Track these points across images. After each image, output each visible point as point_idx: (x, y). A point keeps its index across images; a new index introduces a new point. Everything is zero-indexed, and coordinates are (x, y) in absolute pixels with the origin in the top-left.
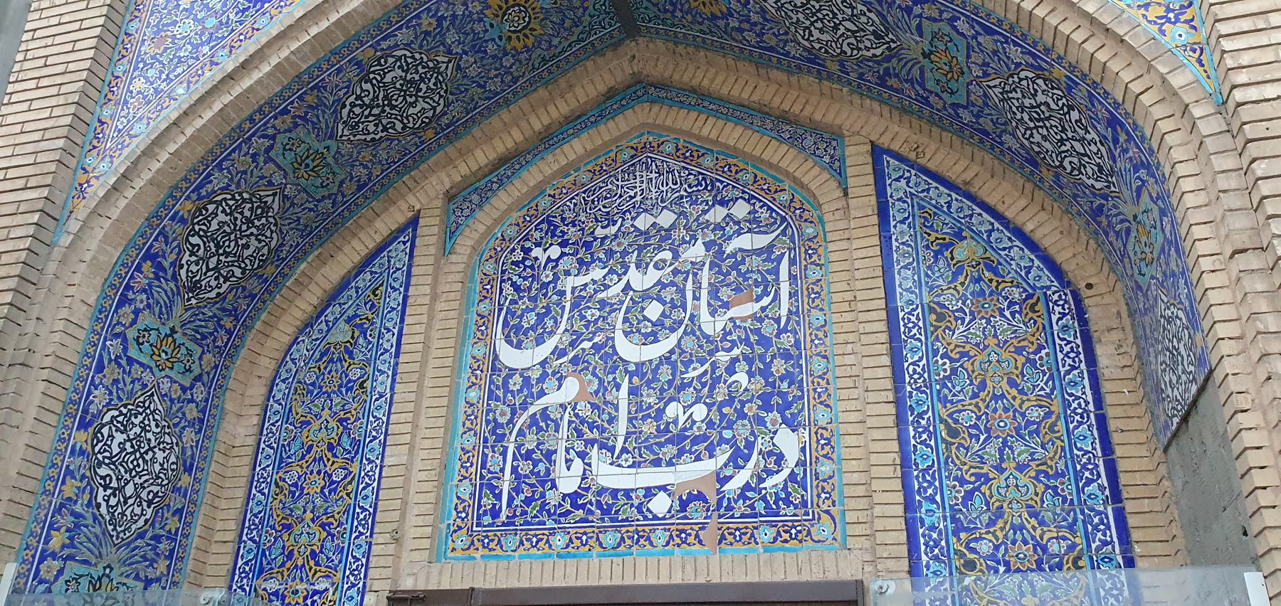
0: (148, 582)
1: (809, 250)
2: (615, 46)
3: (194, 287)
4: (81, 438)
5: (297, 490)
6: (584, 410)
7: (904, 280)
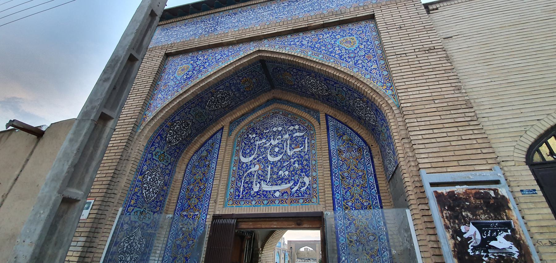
0: (154, 213)
1: (312, 137)
2: (270, 91)
3: (170, 142)
4: (140, 177)
6: (260, 172)
7: (332, 143)
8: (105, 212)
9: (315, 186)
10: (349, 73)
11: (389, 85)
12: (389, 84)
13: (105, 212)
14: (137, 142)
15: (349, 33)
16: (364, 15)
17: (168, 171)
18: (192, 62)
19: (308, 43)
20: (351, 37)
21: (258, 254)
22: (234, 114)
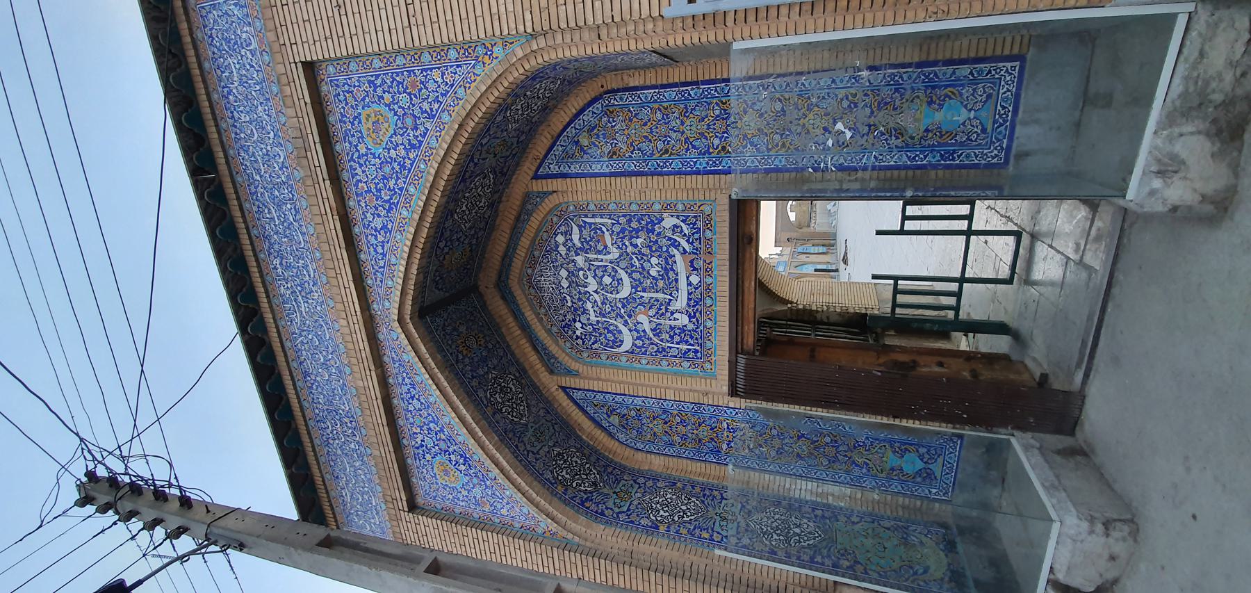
0: (723, 498)
1: (582, 210)
2: (481, 295)
3: (595, 484)
4: (662, 528)
5: (684, 437)
6: (652, 312)
7: (597, 168)
8: (723, 576)
9: (680, 207)
10: (452, 133)
11: (480, 50)
12: (479, 49)
13: (723, 576)
14: (597, 541)
15: (353, 124)
16: (305, 87)
17: (650, 483)
18: (428, 457)
19: (379, 216)
20: (363, 120)
21: (798, 310)
22: (532, 367)
